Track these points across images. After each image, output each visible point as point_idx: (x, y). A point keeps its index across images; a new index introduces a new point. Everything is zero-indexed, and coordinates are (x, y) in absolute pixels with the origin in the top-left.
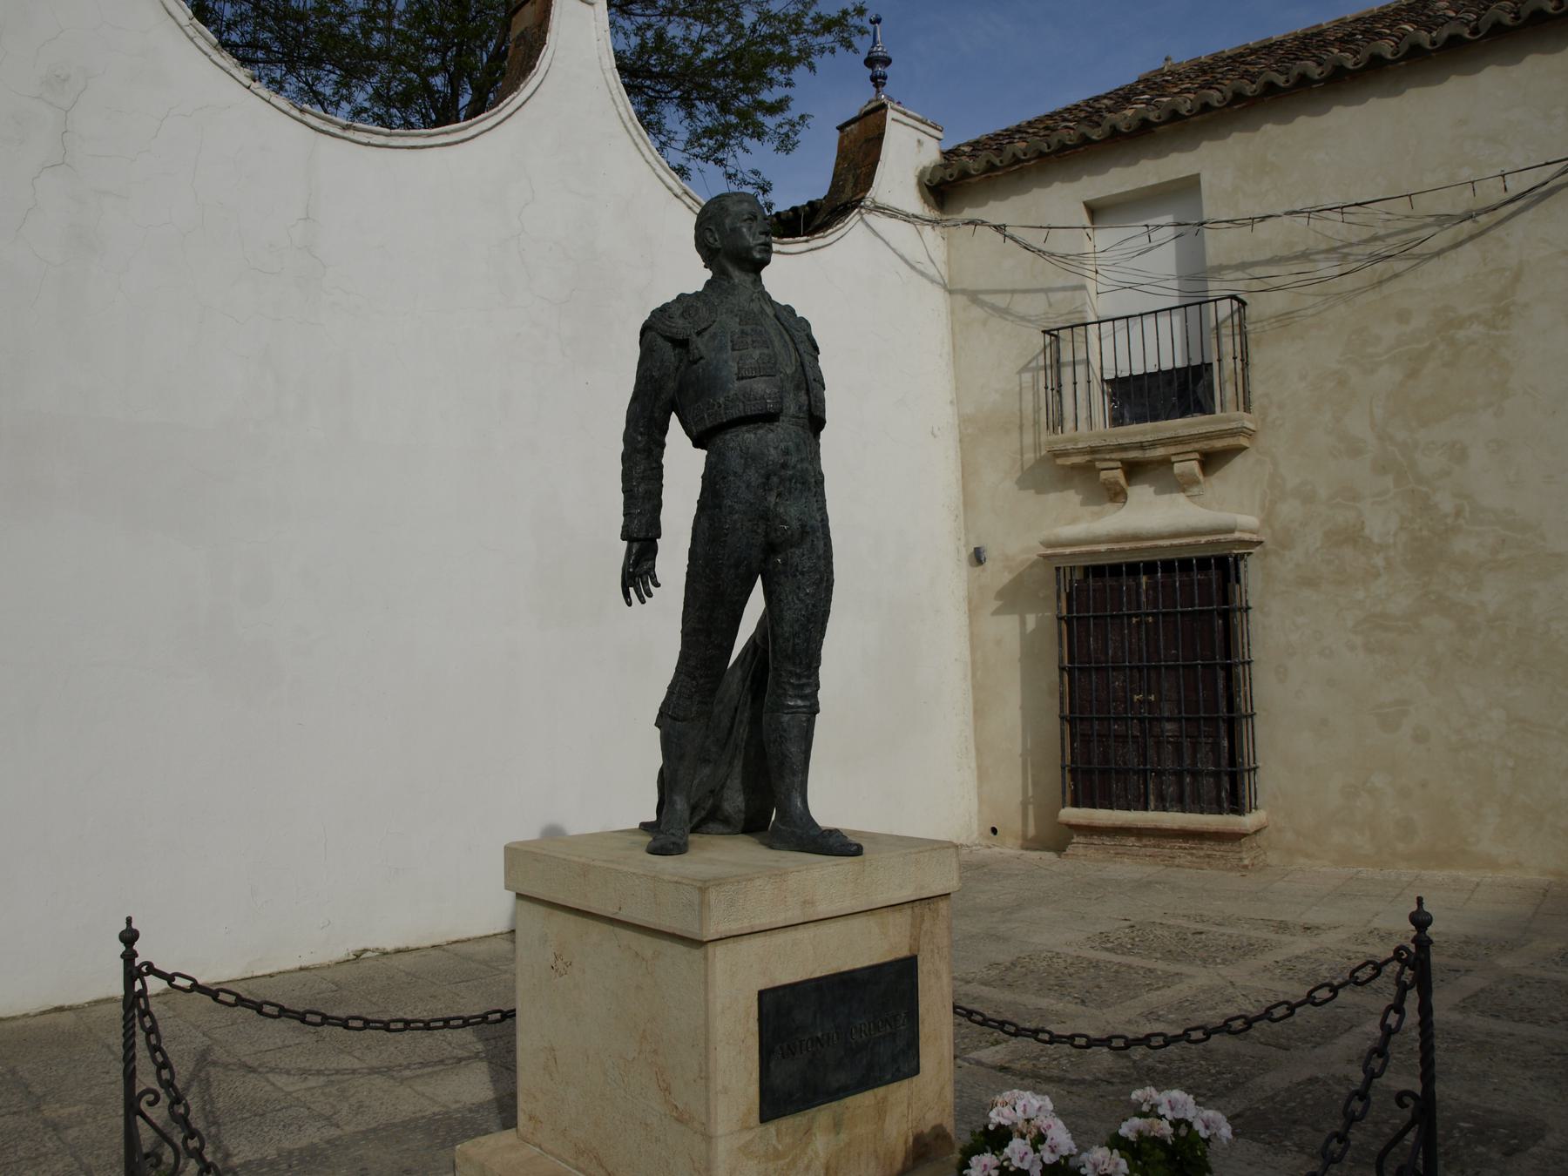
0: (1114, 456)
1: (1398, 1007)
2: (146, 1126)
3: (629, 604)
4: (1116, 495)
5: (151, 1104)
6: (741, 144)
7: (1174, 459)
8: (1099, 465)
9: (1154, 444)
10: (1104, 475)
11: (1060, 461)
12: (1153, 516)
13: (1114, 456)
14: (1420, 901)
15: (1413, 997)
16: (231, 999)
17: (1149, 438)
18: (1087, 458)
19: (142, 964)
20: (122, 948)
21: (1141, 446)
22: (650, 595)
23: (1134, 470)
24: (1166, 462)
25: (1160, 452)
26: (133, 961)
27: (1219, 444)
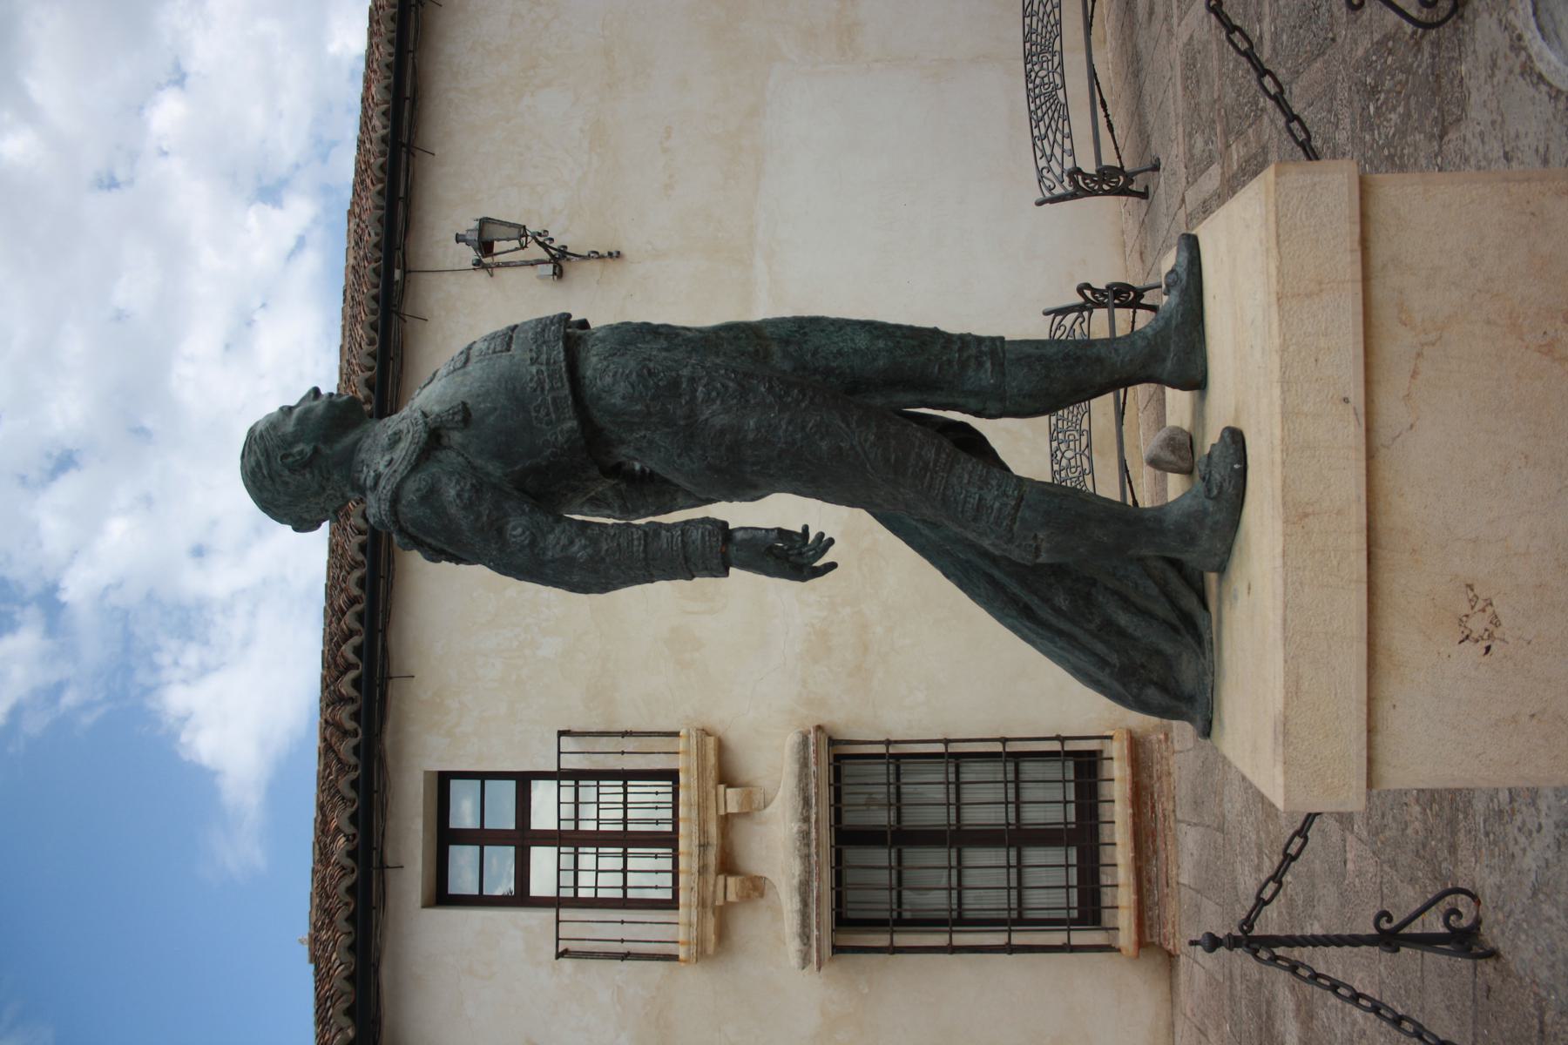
0: (711, 882)
1: (1294, 968)
2: (1418, 921)
3: (833, 566)
4: (756, 887)
5: (1390, 920)
6: (371, 369)
7: (722, 812)
8: (720, 902)
9: (703, 831)
10: (732, 897)
11: (710, 948)
12: (779, 844)
13: (711, 882)
14: (1193, 943)
15: (1279, 951)
16: (1272, 886)
17: (695, 829)
18: (710, 914)
19: (1241, 929)
20: (1222, 951)
21: (703, 846)
22: (821, 535)
23: (728, 865)
24: (726, 821)
25: (713, 829)
26: (1235, 938)
27: (712, 759)
